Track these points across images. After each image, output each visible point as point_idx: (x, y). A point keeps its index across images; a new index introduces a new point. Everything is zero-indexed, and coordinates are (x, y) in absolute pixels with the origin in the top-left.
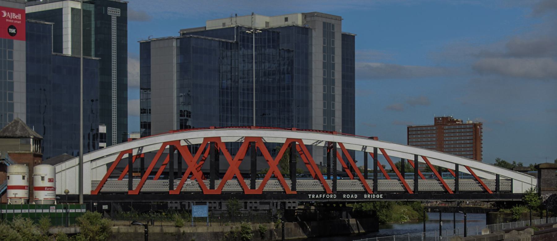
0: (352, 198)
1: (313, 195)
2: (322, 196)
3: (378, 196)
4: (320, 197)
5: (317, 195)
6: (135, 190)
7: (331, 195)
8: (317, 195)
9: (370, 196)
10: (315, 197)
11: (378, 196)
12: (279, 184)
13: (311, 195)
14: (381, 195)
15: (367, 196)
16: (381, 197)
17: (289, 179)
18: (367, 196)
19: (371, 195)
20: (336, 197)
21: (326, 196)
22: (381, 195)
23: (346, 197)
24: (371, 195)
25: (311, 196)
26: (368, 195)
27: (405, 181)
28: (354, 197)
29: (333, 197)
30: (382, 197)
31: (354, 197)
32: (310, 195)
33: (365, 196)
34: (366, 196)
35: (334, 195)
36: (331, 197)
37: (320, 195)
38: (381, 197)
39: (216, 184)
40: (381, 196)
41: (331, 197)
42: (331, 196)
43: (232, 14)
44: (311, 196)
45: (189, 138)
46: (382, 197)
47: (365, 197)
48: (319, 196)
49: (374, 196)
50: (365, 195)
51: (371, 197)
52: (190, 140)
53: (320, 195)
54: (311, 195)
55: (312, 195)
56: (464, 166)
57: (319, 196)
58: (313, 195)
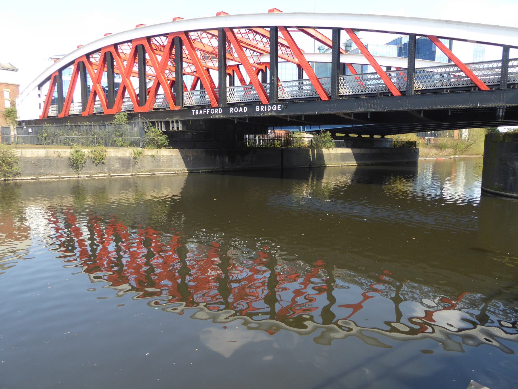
2: (206, 111)
3: (274, 107)
9: (264, 109)
10: (199, 113)
15: (260, 108)
16: (278, 110)
18: (260, 108)
21: (210, 111)
22: (278, 105)
23: (233, 111)
25: (195, 112)
26: (261, 106)
29: (218, 112)
32: (193, 111)
33: (257, 109)
34: (258, 109)
40: (279, 107)
43: (19, 117)
44: (195, 112)
46: (280, 109)
47: (257, 111)
48: (203, 112)
51: (266, 110)
55: (195, 111)
57: (203, 112)
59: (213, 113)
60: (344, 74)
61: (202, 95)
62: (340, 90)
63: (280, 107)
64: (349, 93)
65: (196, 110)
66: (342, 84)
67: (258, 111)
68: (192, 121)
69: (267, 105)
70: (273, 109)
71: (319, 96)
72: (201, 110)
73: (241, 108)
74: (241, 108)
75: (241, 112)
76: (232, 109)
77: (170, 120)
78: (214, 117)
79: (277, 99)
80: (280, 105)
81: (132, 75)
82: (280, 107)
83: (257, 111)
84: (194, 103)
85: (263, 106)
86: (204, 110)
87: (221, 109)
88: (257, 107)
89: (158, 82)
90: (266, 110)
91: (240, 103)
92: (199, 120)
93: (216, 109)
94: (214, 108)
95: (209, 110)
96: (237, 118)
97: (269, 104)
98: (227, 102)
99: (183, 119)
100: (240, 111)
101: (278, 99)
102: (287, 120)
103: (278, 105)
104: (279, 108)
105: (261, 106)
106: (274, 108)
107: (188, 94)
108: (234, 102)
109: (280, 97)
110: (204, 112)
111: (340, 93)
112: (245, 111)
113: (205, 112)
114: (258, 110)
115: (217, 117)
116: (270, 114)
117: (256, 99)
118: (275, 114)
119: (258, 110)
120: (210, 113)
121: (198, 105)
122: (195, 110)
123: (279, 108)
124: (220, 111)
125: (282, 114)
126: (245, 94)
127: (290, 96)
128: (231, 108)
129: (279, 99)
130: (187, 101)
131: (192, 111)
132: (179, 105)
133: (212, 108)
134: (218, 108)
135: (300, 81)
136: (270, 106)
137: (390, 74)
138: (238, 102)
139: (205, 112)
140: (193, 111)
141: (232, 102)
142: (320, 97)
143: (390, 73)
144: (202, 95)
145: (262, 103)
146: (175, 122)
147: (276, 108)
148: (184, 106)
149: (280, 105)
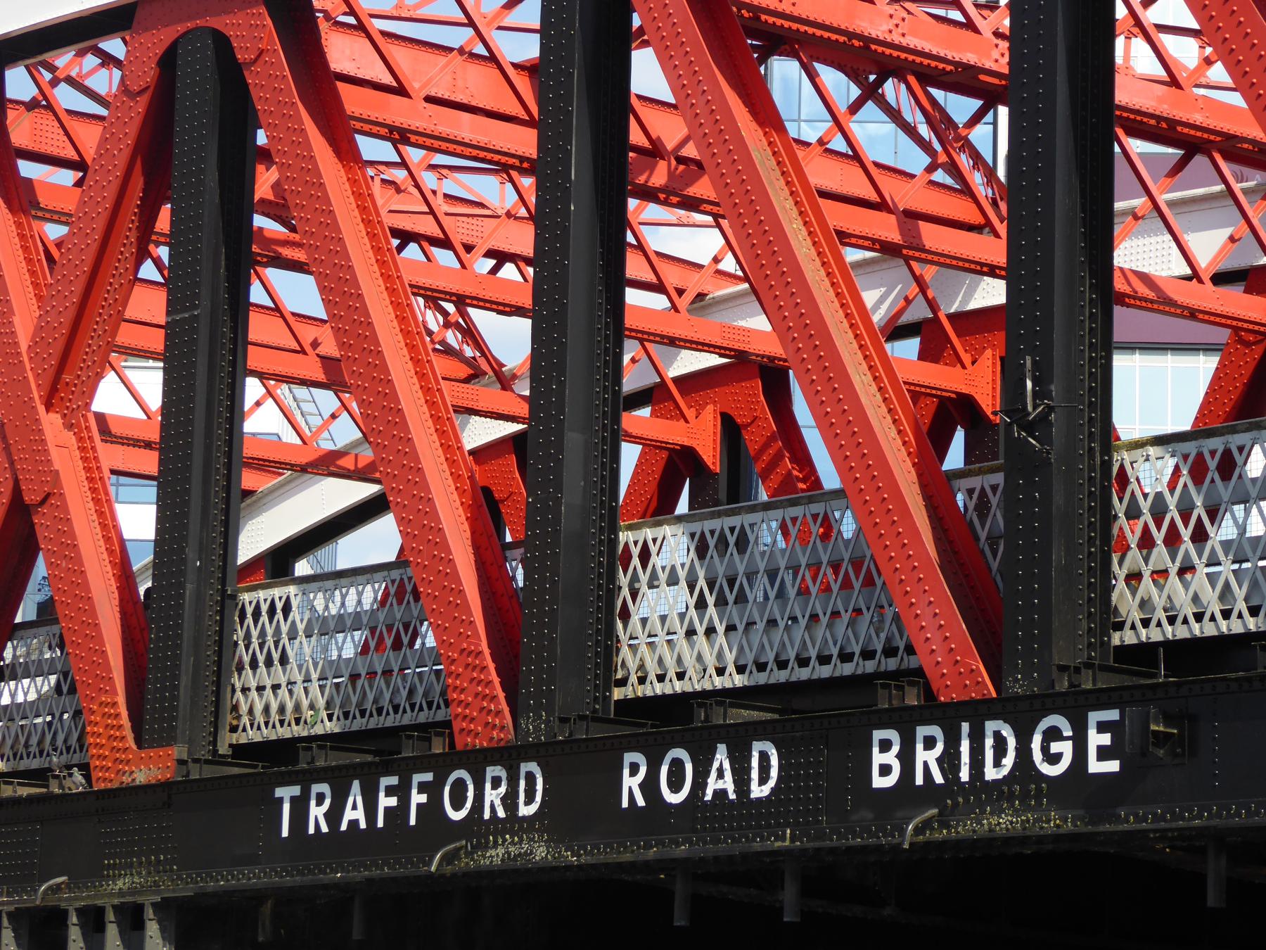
2: (402, 792)
3: (1053, 734)
9: (949, 761)
10: (334, 815)
15: (907, 757)
16: (1095, 766)
18: (907, 757)
22: (1094, 717)
23: (650, 787)
26: (922, 731)
29: (510, 801)
30: (1113, 766)
31: (742, 782)
32: (286, 793)
33: (878, 758)
34: (891, 758)
38: (1095, 766)
40: (1097, 739)
46: (1113, 766)
47: (879, 782)
51: (964, 775)
59: (456, 816)
60: (734, 496)
61: (398, 613)
62: (1124, 600)
63: (1106, 739)
64: (1226, 614)
65: (317, 788)
66: (1186, 519)
67: (890, 781)
68: (286, 899)
69: (978, 712)
70: (1037, 756)
71: (913, 662)
72: (356, 785)
73: (721, 757)
74: (721, 757)
75: (720, 794)
76: (634, 769)
77: (73, 902)
78: (464, 863)
79: (1105, 645)
80: (1113, 715)
81: (120, 339)
82: (1106, 739)
83: (879, 782)
84: (321, 703)
85: (935, 731)
86: (386, 781)
87: (533, 767)
88: (878, 735)
89: (17, 493)
90: (964, 775)
91: (715, 693)
92: (344, 895)
93: (492, 771)
94: (477, 761)
95: (428, 777)
96: (694, 869)
97: (1001, 708)
98: (618, 694)
99: (185, 890)
100: (712, 785)
101: (1116, 639)
102: (780, 911)
103: (1094, 717)
104: (1103, 754)
105: (922, 731)
106: (1055, 747)
107: (272, 611)
108: (679, 687)
109: (1136, 616)
110: (386, 801)
111: (1120, 626)
112: (758, 791)
113: (393, 801)
114: (885, 770)
115: (495, 855)
116: (1004, 822)
117: (868, 654)
118: (1055, 822)
119: (885, 770)
120: (432, 810)
121: (358, 724)
122: (305, 779)
123: (1103, 754)
124: (530, 800)
125: (1128, 821)
126: (1213, 513)
127: (1241, 606)
128: (629, 757)
129: (1129, 638)
130: (260, 689)
131: (279, 792)
132: (167, 739)
133: (457, 758)
134: (509, 756)
135: (708, 525)
136: (1007, 732)
137: (1227, 454)
138: (718, 682)
139: (393, 801)
140: (286, 793)
141: (659, 689)
142: (919, 672)
143: (748, 518)
144: (398, 613)
145: (929, 694)
146: (110, 916)
147: (1065, 748)
148: (226, 741)
149: (1113, 715)
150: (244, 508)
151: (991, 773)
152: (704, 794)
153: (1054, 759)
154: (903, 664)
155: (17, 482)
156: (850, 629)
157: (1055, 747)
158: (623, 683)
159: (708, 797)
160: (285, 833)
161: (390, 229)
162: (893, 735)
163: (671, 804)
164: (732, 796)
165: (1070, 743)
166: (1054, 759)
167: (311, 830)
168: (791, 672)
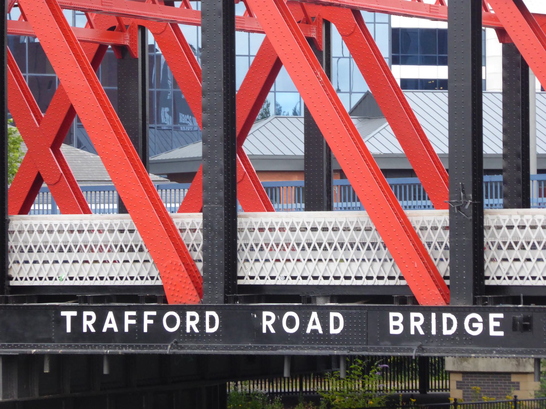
0: (315, 331)
1: (86, 314)
2: (140, 319)
3: (474, 320)
4: (126, 330)
5: (111, 315)
6: (407, 282)
7: (189, 314)
8: (111, 315)
9: (426, 326)
10: (99, 324)
11: (474, 320)
12: (379, 240)
13: (75, 313)
14: (492, 316)
16: (492, 333)
17: (303, 206)
19: (434, 315)
20: (338, 331)
21: (158, 319)
22: (492, 316)
23: (277, 324)
24: (434, 315)
25: (77, 321)
26: (413, 315)
27: (110, 175)
28: (325, 325)
29: (201, 325)
30: (501, 334)
31: (325, 325)
32: (69, 315)
33: (392, 323)
34: (399, 323)
35: (208, 314)
36: (191, 325)
37: (127, 314)
38: (492, 333)
39: (493, 260)
40: (493, 324)
41: (191, 325)
42: (413, 324)
44: (77, 321)
45: (500, 125)
46: (501, 334)
47: (392, 331)
48: (120, 321)
49: (450, 323)
50: (392, 315)
51: (434, 332)
52: (486, 121)
53: (127, 314)
54: (75, 313)
56: (337, 63)
57: (120, 321)
58: (86, 314)
63: (498, 324)
82: (498, 324)
83: (392, 331)
90: (434, 332)
104: (496, 329)
106: (475, 325)
119: (396, 328)
123: (496, 329)
147: (480, 327)
149: (501, 316)
150: (437, 265)
151: (446, 332)
152: (306, 330)
153: (475, 329)
154: (364, 283)
155: (119, 195)
156: (360, 267)
157: (475, 325)
158: (242, 278)
159: (145, 330)
160: (69, 330)
161: (381, 170)
162: (400, 315)
163: (217, 330)
164: (321, 332)
165: (482, 324)
166: (475, 329)
167: (264, 331)
168: (331, 281)
